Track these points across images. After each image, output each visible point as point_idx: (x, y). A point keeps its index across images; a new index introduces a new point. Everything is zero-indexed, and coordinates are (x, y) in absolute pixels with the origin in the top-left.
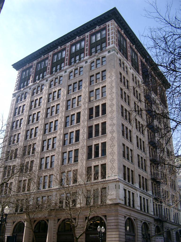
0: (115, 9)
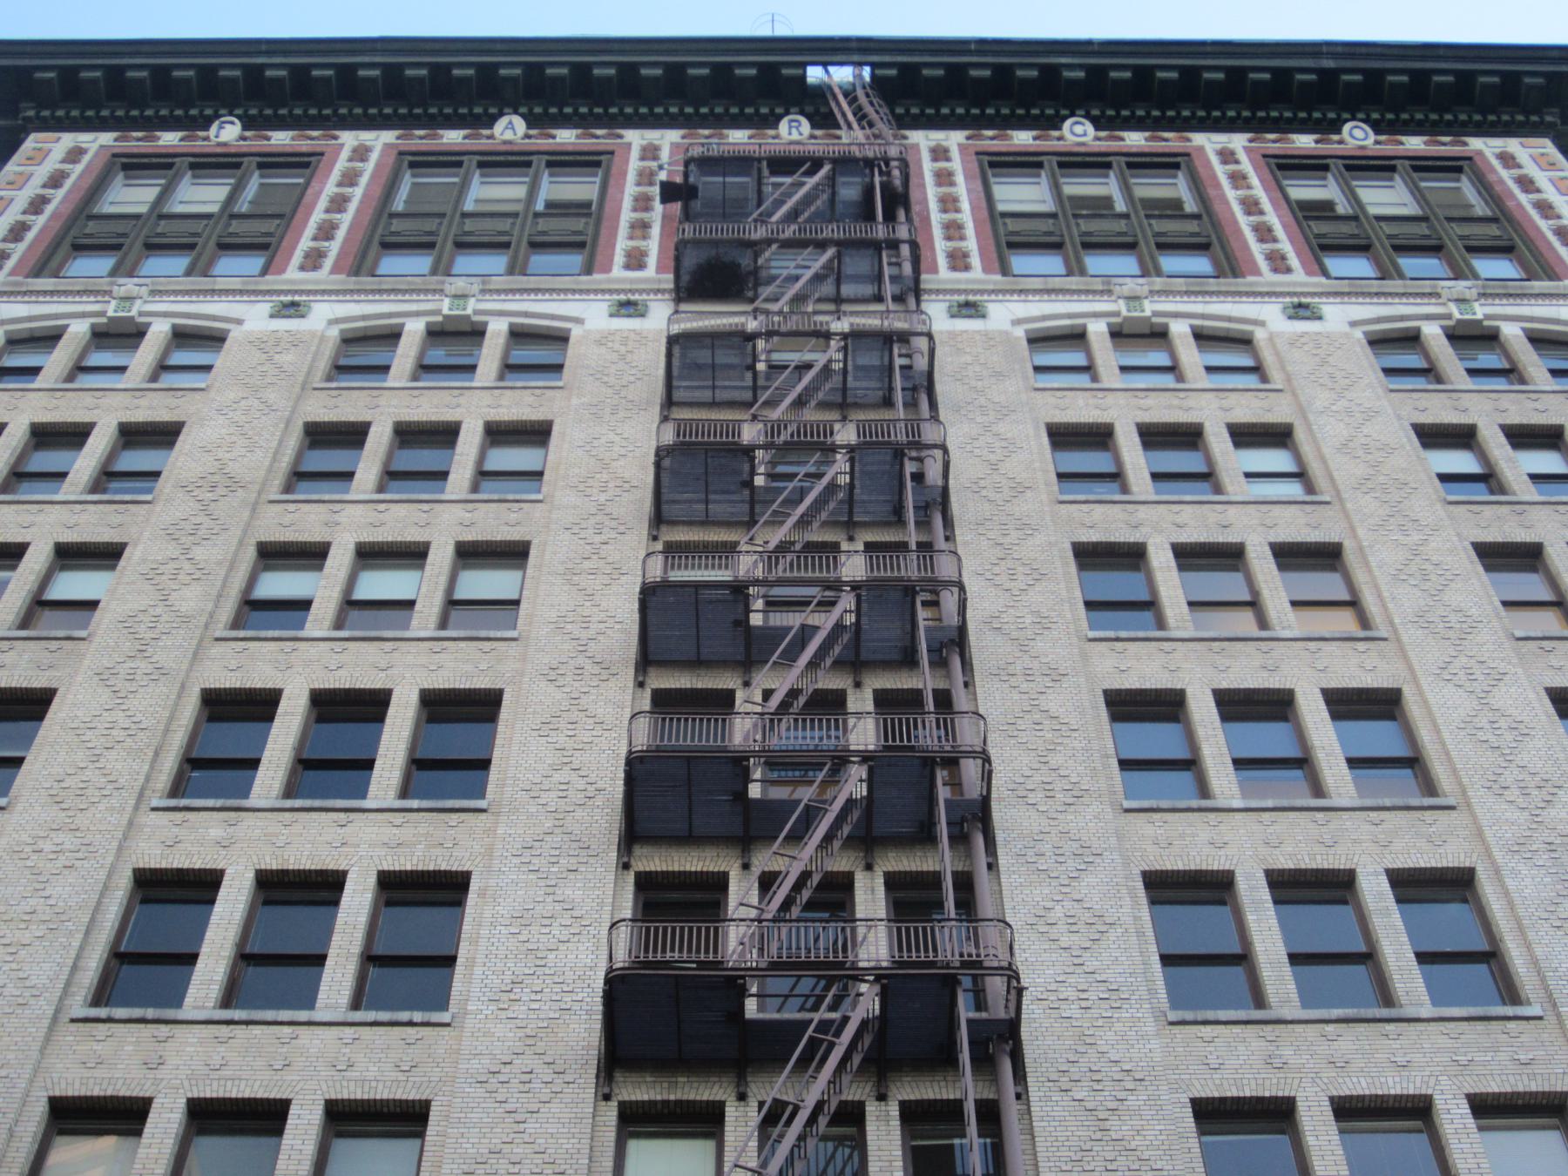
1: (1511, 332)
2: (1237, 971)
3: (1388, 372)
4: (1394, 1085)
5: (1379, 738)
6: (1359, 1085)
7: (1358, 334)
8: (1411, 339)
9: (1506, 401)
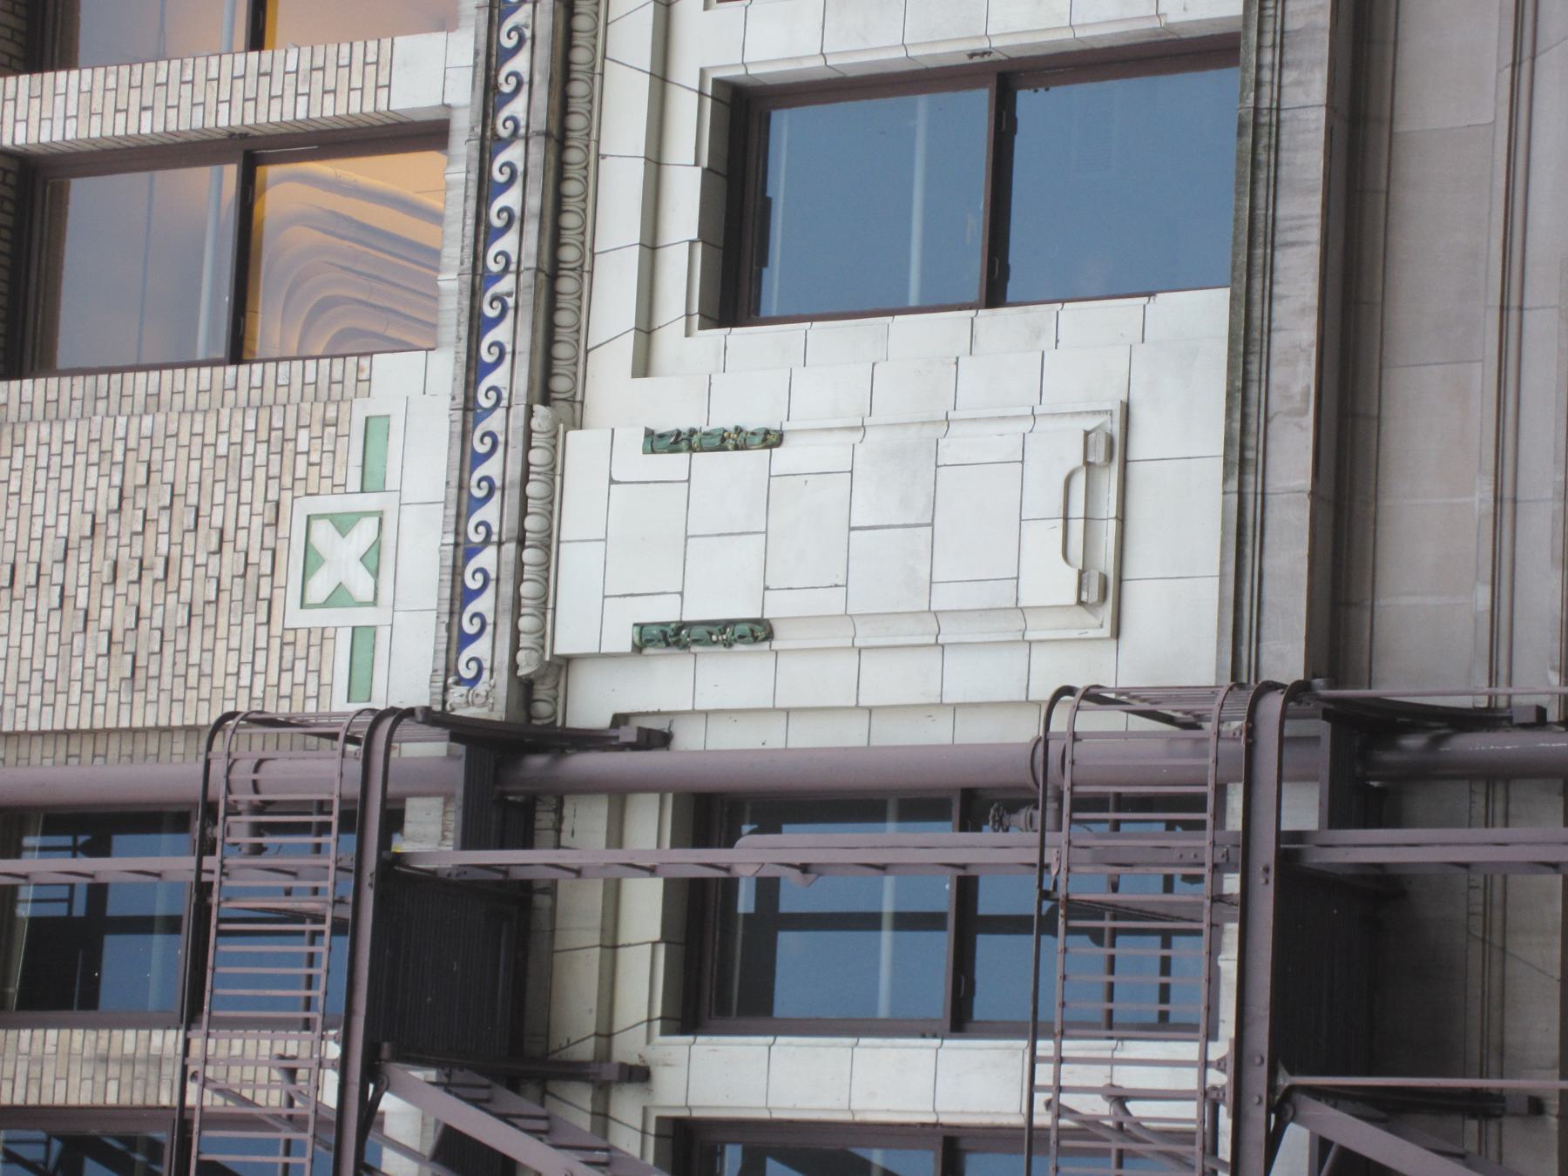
2: (785, 126)
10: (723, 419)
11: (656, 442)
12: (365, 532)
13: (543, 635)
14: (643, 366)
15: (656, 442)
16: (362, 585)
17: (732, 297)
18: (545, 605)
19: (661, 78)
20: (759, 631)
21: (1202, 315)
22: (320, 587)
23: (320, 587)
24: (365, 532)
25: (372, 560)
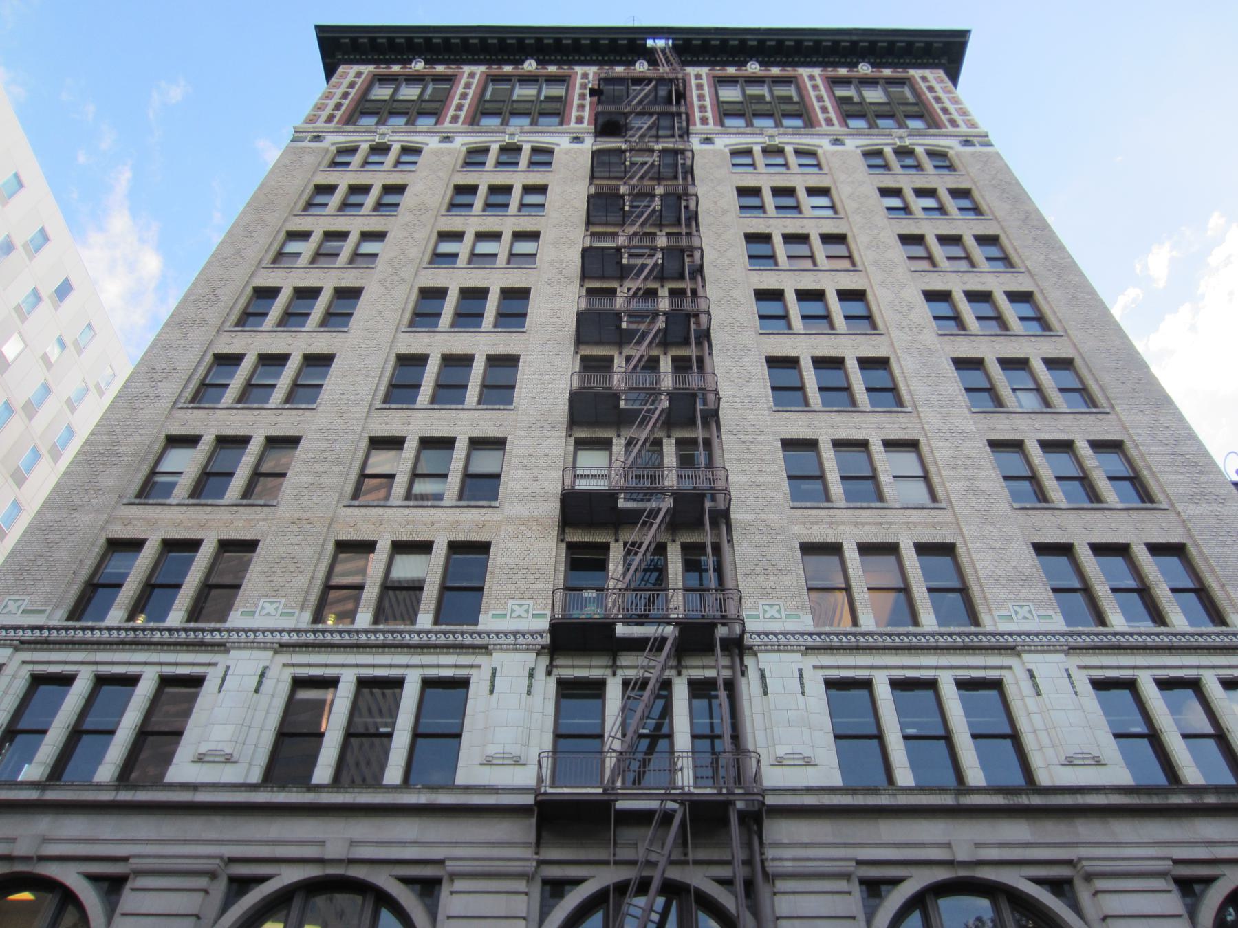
0: (320, 29)
1: (920, 150)
2: (865, 693)
3: (870, 166)
4: (855, 435)
5: (856, 308)
6: (842, 435)
7: (859, 151)
8: (879, 153)
9: (915, 178)
10: (1076, 683)
11: (800, 671)
12: (777, 615)
13: (234, 648)
14: (815, 667)
15: (800, 671)
16: (767, 616)
17: (830, 684)
18: (1030, 651)
19: (937, 668)
20: (766, 693)
21: (837, 780)
22: (766, 608)
23: (766, 608)
24: (777, 615)
25: (773, 617)
